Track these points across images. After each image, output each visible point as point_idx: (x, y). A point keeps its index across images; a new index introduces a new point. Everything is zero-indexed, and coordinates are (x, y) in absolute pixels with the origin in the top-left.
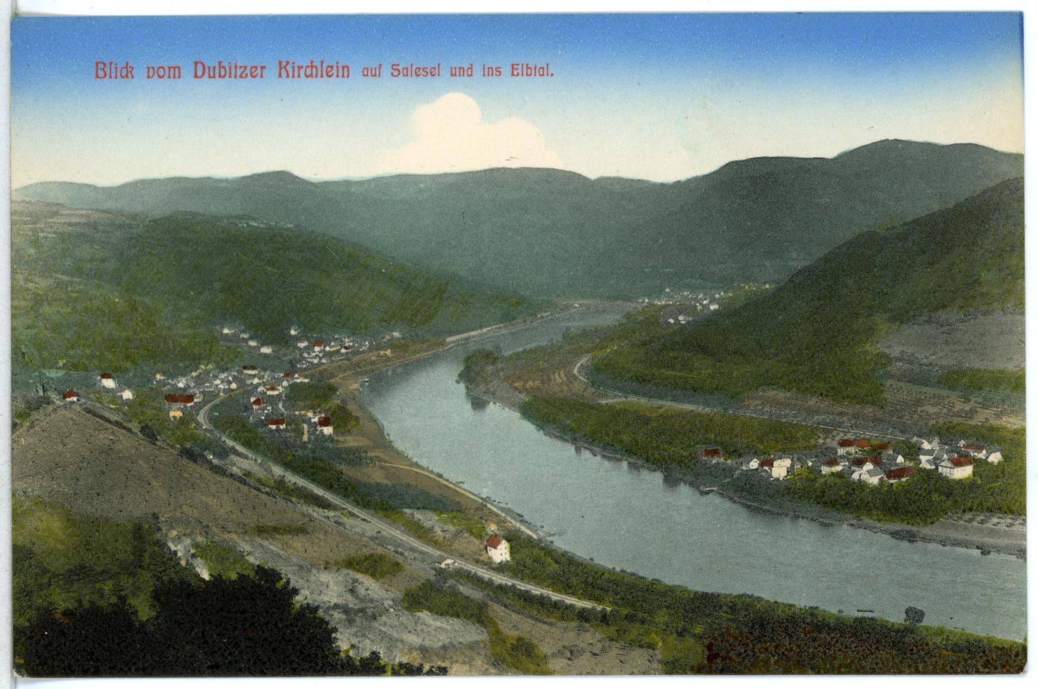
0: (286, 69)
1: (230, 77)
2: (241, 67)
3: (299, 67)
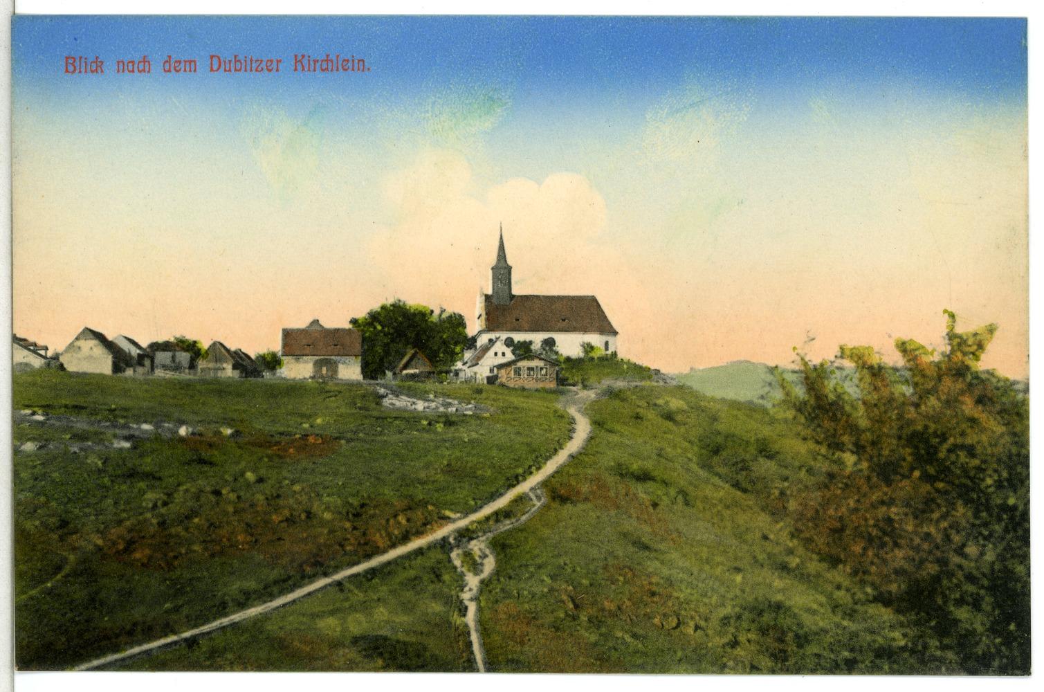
1: (246, 70)
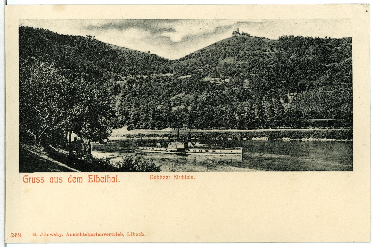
3: (29, 178)
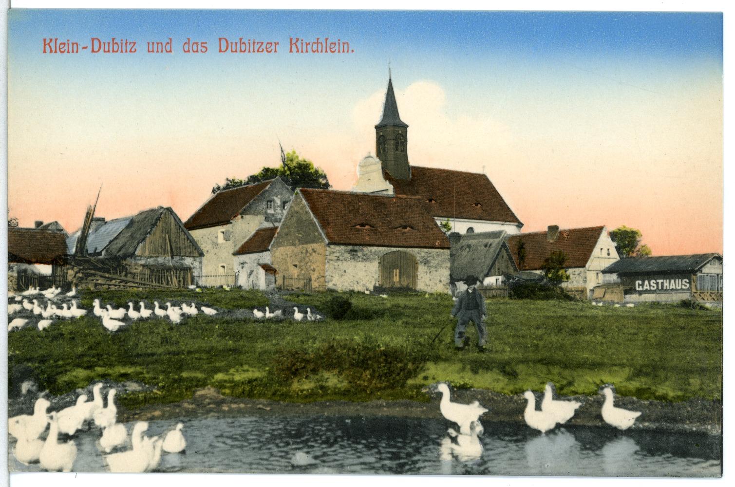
0: (50, 47)
2: (130, 43)
